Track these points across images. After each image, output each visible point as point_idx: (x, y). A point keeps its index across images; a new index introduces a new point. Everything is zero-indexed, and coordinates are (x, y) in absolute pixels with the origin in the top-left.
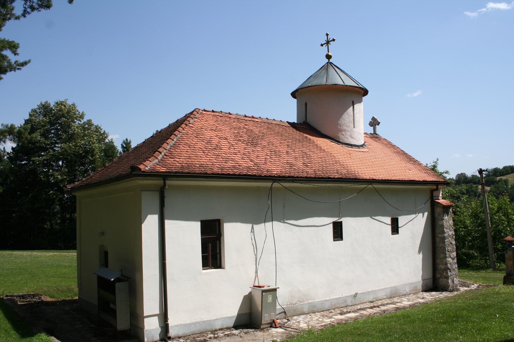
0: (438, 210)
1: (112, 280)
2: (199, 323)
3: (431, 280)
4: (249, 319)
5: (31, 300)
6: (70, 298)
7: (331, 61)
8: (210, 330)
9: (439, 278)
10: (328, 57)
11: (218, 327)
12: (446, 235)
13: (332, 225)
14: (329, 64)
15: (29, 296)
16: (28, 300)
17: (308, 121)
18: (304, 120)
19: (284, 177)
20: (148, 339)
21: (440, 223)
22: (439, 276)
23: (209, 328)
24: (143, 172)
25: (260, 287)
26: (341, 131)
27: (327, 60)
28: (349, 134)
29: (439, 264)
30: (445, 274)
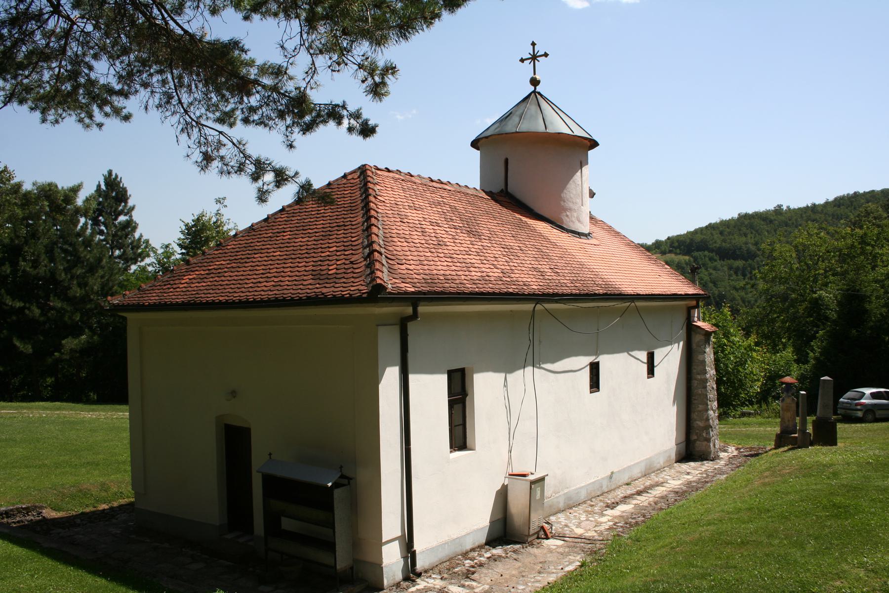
0: (697, 338)
1: (330, 484)
4: (505, 532)
5: (23, 518)
6: (91, 509)
7: (538, 89)
9: (695, 441)
10: (535, 82)
11: (469, 547)
12: (708, 376)
13: (588, 368)
14: (534, 97)
15: (19, 512)
16: (18, 519)
17: (509, 190)
18: (502, 186)
19: (548, 295)
21: (700, 357)
22: (695, 437)
23: (459, 550)
24: (390, 293)
25: (524, 475)
26: (565, 210)
27: (532, 88)
28: (575, 215)
30: (704, 435)
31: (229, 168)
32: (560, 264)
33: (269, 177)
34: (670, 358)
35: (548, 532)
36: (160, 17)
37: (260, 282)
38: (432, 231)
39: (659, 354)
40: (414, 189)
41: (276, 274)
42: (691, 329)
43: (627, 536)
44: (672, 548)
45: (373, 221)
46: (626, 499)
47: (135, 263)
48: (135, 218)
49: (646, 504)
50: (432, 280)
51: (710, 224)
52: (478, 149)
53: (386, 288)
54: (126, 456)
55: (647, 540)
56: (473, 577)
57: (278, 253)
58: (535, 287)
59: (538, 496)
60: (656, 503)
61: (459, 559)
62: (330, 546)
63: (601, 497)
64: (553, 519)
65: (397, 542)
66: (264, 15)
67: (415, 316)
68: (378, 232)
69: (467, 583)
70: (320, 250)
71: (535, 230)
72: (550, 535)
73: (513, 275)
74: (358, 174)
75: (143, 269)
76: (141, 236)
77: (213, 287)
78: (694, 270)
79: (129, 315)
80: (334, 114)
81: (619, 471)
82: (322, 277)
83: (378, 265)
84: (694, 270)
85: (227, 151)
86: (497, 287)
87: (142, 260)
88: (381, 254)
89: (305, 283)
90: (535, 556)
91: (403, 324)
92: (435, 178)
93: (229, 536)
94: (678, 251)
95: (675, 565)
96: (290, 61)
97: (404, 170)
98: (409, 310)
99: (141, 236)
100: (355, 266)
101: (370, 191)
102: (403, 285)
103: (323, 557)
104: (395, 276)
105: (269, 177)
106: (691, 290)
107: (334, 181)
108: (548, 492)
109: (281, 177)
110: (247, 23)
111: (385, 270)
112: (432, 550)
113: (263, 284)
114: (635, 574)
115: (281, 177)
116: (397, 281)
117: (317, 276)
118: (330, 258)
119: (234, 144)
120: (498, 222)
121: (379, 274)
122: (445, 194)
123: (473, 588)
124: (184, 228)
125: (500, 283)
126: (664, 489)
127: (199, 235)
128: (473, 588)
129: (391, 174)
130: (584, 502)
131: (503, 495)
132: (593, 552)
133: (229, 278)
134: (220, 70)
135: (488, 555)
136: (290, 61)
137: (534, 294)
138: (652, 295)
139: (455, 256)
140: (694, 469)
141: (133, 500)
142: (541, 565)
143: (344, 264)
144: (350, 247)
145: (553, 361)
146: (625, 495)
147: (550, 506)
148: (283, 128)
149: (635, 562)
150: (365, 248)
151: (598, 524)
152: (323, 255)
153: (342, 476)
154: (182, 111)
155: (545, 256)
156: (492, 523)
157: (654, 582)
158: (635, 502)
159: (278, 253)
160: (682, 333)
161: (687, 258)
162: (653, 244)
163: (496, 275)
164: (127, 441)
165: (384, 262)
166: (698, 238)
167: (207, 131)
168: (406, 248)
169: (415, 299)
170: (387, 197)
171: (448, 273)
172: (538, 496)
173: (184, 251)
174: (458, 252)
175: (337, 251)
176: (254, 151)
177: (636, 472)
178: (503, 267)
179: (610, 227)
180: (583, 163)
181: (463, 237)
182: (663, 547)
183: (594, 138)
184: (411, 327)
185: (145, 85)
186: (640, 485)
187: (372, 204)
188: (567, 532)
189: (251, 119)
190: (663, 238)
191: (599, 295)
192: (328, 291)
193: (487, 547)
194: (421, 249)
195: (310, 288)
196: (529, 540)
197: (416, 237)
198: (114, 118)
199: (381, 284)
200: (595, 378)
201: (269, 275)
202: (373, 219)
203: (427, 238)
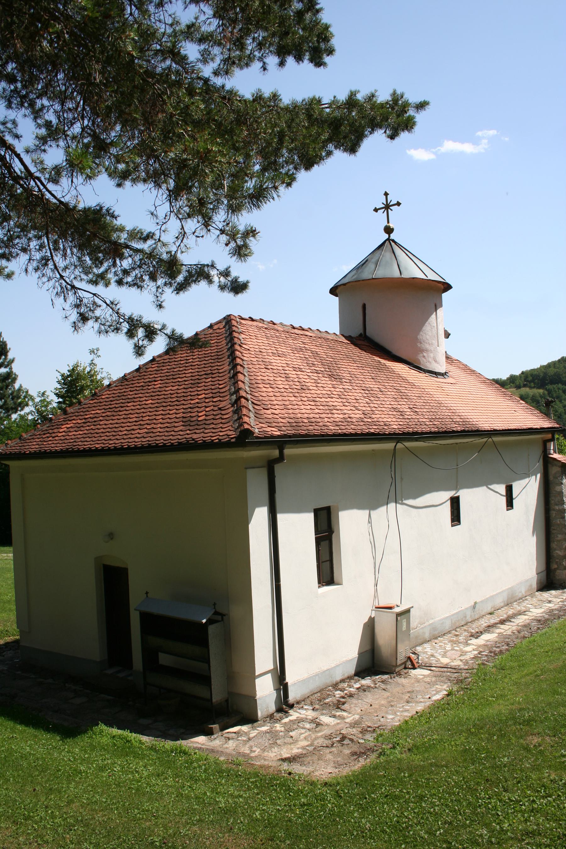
0: (554, 470)
1: (204, 621)
2: (317, 675)
3: (545, 573)
4: (374, 663)
7: (393, 236)
8: (330, 684)
9: (555, 569)
10: (389, 230)
11: (338, 678)
14: (389, 244)
18: (360, 330)
19: (408, 434)
20: (262, 713)
22: (556, 566)
24: (257, 437)
25: (390, 608)
26: (422, 351)
27: (386, 236)
28: (432, 355)
29: (555, 550)
31: (106, 327)
32: (419, 403)
33: (141, 332)
34: (528, 490)
35: (415, 662)
36: (36, 189)
37: (133, 430)
38: (295, 376)
39: (517, 486)
40: (277, 337)
41: (148, 422)
42: (547, 462)
43: (491, 664)
44: (537, 676)
45: (239, 368)
46: (489, 628)
47: (16, 412)
48: (14, 370)
49: (509, 633)
50: (297, 424)
51: (563, 358)
52: (336, 296)
53: (253, 433)
54: (11, 595)
55: (511, 668)
56: (343, 707)
57: (150, 401)
58: (396, 427)
59: (404, 628)
60: (519, 632)
61: (329, 690)
62: (206, 680)
63: (464, 627)
64: (419, 649)
65: (269, 675)
66: (134, 181)
67: (281, 458)
68: (244, 379)
69: (338, 714)
70: (189, 398)
71: (393, 372)
72: (416, 665)
73: (373, 416)
74: (224, 324)
75: (22, 417)
76: (21, 386)
77: (90, 435)
78: (548, 404)
79: (13, 464)
80: (200, 273)
81: (482, 602)
82: (192, 424)
83: (244, 411)
84: (548, 404)
85: (103, 312)
86: (359, 427)
87: (22, 410)
88: (247, 400)
89: (176, 429)
90: (403, 686)
91: (271, 467)
92: (296, 325)
93: (110, 671)
94: (532, 385)
95: (540, 693)
96: (163, 228)
97: (267, 319)
98: (276, 453)
99: (21, 386)
100: (223, 412)
101: (236, 340)
102: (269, 429)
103: (199, 690)
104: (261, 420)
105: (141, 332)
106: (546, 424)
107: (201, 332)
108: (413, 624)
109: (151, 333)
110: (120, 190)
111: (251, 415)
112: (304, 682)
113: (137, 431)
114: (501, 702)
115: (151, 333)
116: (263, 425)
117: (188, 422)
118: (200, 405)
119: (107, 305)
120: (358, 365)
121: (246, 419)
122: (307, 340)
123: (344, 718)
124: (60, 378)
125: (362, 423)
126: (526, 617)
127: (74, 385)
128: (344, 718)
129: (255, 323)
130: (449, 632)
131: (370, 628)
132: (459, 681)
133: (104, 426)
134: (92, 235)
135: (357, 685)
136: (163, 228)
137: (395, 434)
138: (509, 430)
139: (318, 399)
140: (556, 597)
141: (18, 637)
142: (409, 695)
143: (213, 410)
144: (218, 394)
145: (415, 497)
146: (489, 624)
147: (417, 637)
148: (154, 289)
149: (500, 690)
150: (232, 395)
151: (463, 653)
152: (192, 402)
153: (216, 613)
154: (58, 276)
155: (404, 396)
156: (361, 654)
157: (520, 710)
158: (498, 631)
159: (150, 401)
160: (539, 465)
161: (541, 391)
162: (508, 379)
163: (358, 416)
164: (11, 582)
165: (250, 407)
166: (552, 371)
167: (81, 293)
168: (271, 394)
169: (281, 442)
170: (251, 344)
171: (311, 416)
172: (404, 628)
173: (61, 400)
174: (321, 396)
175: (206, 398)
176: (126, 310)
177: (499, 602)
178: (364, 409)
179: (466, 366)
180: (437, 305)
181: (325, 381)
182: (527, 675)
183: (448, 281)
184: (278, 469)
185: (24, 250)
186: (503, 614)
187: (237, 353)
188: (433, 661)
189: (125, 281)
190: (517, 373)
191: (457, 432)
192: (198, 437)
193: (356, 678)
194: (285, 394)
195: (182, 434)
196: (397, 670)
197: (280, 382)
198: (14, 372)
199: (248, 429)
200: (455, 512)
201: (142, 423)
202: (239, 367)
203: (291, 383)
